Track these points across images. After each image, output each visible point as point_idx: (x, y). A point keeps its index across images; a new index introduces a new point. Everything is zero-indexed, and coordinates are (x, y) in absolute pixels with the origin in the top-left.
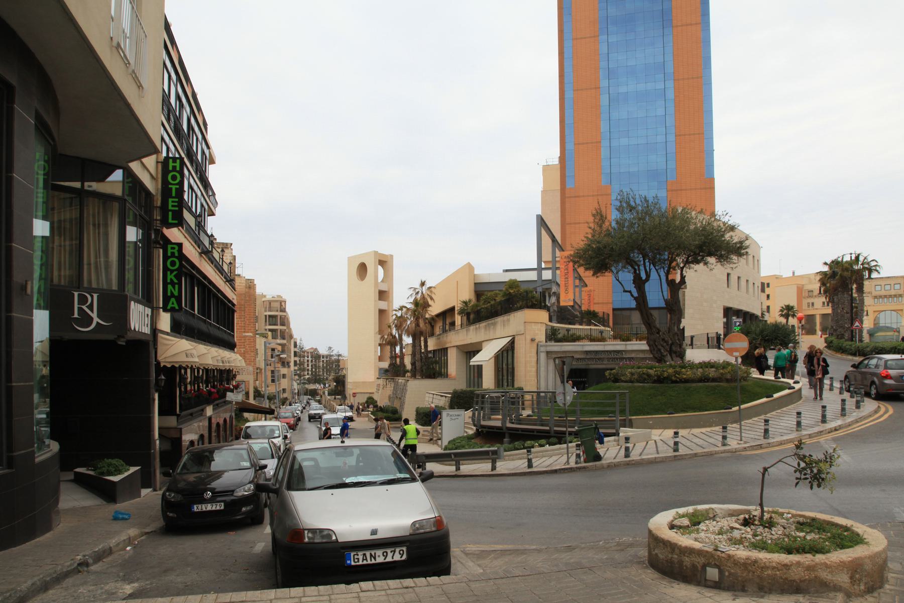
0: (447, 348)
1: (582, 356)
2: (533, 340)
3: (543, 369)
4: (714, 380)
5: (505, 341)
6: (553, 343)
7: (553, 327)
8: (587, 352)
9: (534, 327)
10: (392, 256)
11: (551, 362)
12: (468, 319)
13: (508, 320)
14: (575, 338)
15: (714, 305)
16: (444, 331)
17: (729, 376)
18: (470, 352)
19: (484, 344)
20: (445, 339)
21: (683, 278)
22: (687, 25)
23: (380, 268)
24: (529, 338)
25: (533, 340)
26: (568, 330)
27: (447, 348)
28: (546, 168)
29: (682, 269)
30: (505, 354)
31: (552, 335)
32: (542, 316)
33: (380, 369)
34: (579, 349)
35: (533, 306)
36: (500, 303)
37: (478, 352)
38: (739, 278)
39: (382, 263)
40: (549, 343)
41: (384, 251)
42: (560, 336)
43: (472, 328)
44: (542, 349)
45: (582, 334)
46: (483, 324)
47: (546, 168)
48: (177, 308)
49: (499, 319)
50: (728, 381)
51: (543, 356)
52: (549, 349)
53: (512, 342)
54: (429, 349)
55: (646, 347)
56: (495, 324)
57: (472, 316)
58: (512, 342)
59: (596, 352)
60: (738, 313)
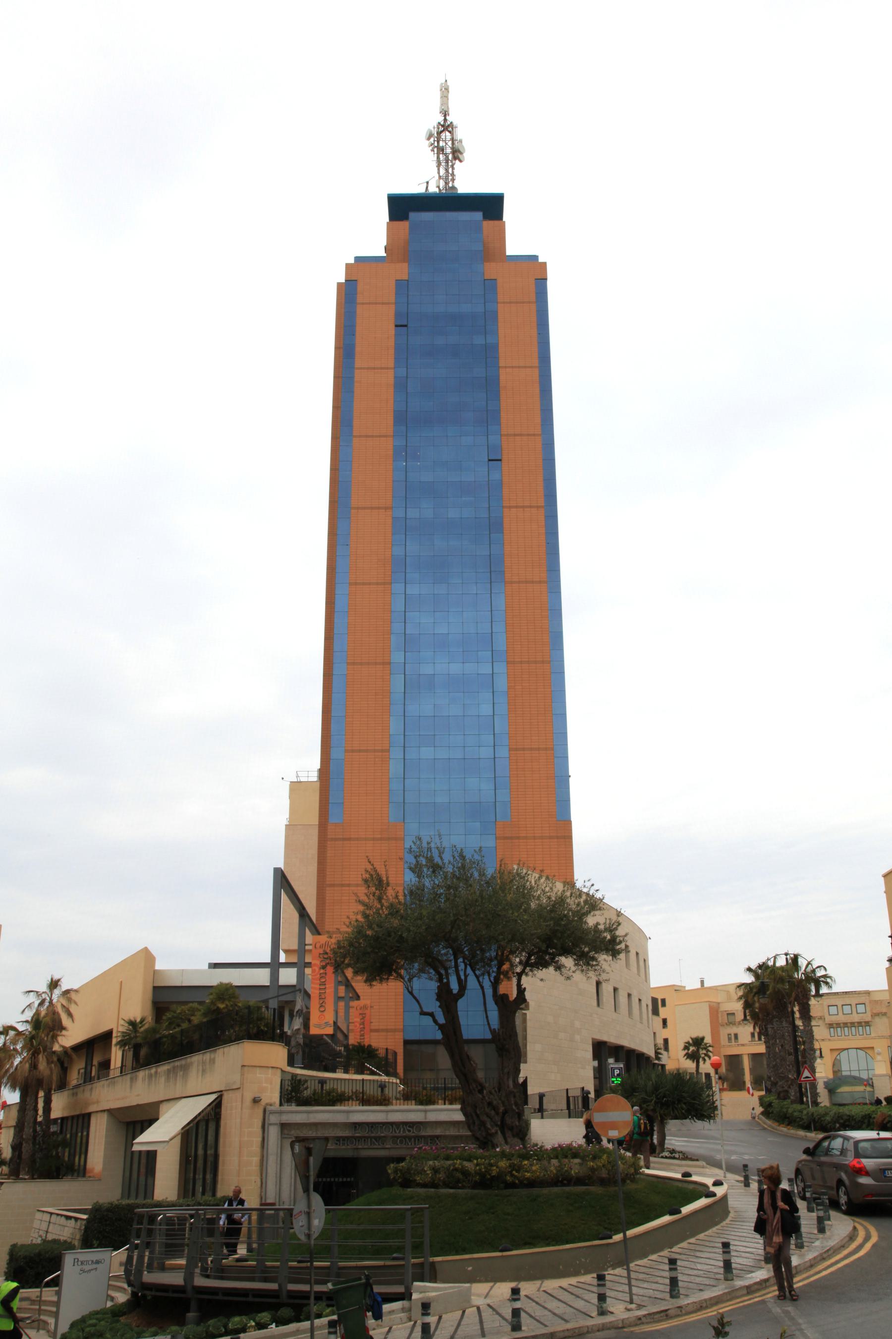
1: (347, 1133)
2: (256, 1101)
4: (580, 1181)
5: (204, 1102)
6: (294, 1108)
7: (294, 1076)
8: (356, 1125)
9: (260, 1075)
12: (136, 1056)
13: (213, 1061)
14: (334, 1098)
16: (88, 1079)
18: (134, 1123)
19: (163, 1107)
20: (87, 1094)
21: (521, 991)
26: (322, 1082)
28: (296, 787)
30: (202, 1128)
31: (293, 1093)
34: (340, 1118)
36: (199, 1027)
37: (157, 1119)
40: (286, 1108)
42: (307, 1093)
43: (142, 1074)
44: (273, 1119)
45: (348, 1090)
46: (164, 1068)
49: (196, 1059)
51: (274, 1133)
54: (54, 1115)
56: (186, 1068)
57: (143, 1052)
58: (216, 1109)
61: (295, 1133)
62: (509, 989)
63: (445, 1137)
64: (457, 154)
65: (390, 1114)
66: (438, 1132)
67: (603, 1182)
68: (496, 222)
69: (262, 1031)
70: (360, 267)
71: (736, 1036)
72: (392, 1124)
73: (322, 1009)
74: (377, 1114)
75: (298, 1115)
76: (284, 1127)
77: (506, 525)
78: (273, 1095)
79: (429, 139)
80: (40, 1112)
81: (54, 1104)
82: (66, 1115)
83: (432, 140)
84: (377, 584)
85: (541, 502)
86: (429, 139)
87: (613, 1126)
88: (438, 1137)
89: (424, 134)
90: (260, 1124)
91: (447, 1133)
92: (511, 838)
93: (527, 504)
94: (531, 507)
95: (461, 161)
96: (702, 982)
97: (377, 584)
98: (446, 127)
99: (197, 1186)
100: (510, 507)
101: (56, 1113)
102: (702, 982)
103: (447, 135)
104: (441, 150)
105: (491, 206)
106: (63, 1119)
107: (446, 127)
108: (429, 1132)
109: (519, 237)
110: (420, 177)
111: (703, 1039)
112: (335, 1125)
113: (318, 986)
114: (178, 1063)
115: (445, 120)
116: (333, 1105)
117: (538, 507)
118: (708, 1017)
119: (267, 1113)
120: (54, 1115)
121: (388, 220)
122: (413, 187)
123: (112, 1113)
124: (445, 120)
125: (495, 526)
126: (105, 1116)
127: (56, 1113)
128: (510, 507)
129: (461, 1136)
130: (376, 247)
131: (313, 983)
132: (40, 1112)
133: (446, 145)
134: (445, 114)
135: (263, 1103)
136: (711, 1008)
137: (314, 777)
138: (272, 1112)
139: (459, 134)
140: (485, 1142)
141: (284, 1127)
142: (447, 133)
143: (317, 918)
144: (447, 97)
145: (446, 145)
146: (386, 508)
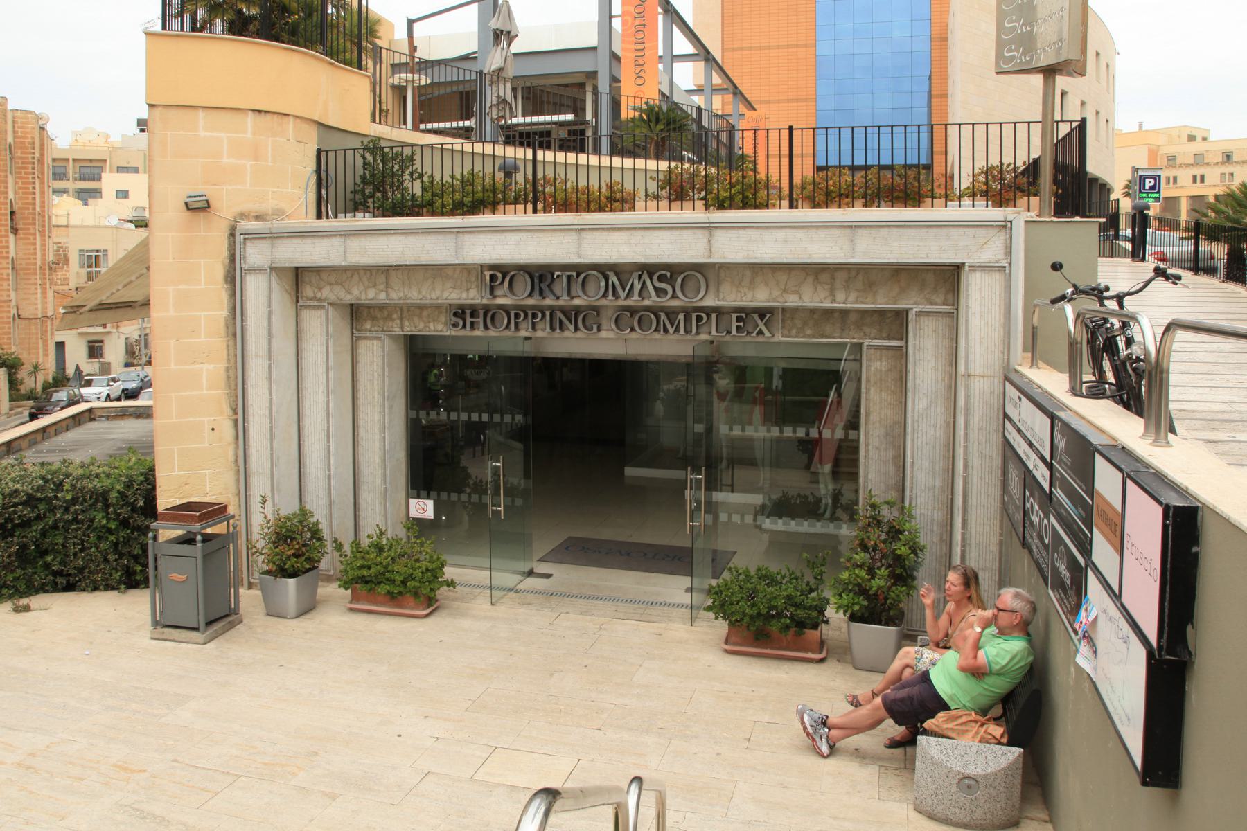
1: (473, 296)
8: (499, 274)
44: (256, 254)
63: (789, 314)
65: (588, 237)
66: (760, 297)
71: (1175, 178)
72: (603, 269)
73: (639, 81)
74: (547, 238)
88: (762, 313)
90: (219, 272)
91: (792, 301)
96: (1141, 126)
102: (1141, 126)
108: (729, 297)
111: (225, 507)
112: (436, 271)
113: (633, 47)
116: (418, 215)
119: (239, 239)
129: (844, 313)
131: (623, 42)
136: (1150, 151)
138: (250, 237)
143: (695, 15)
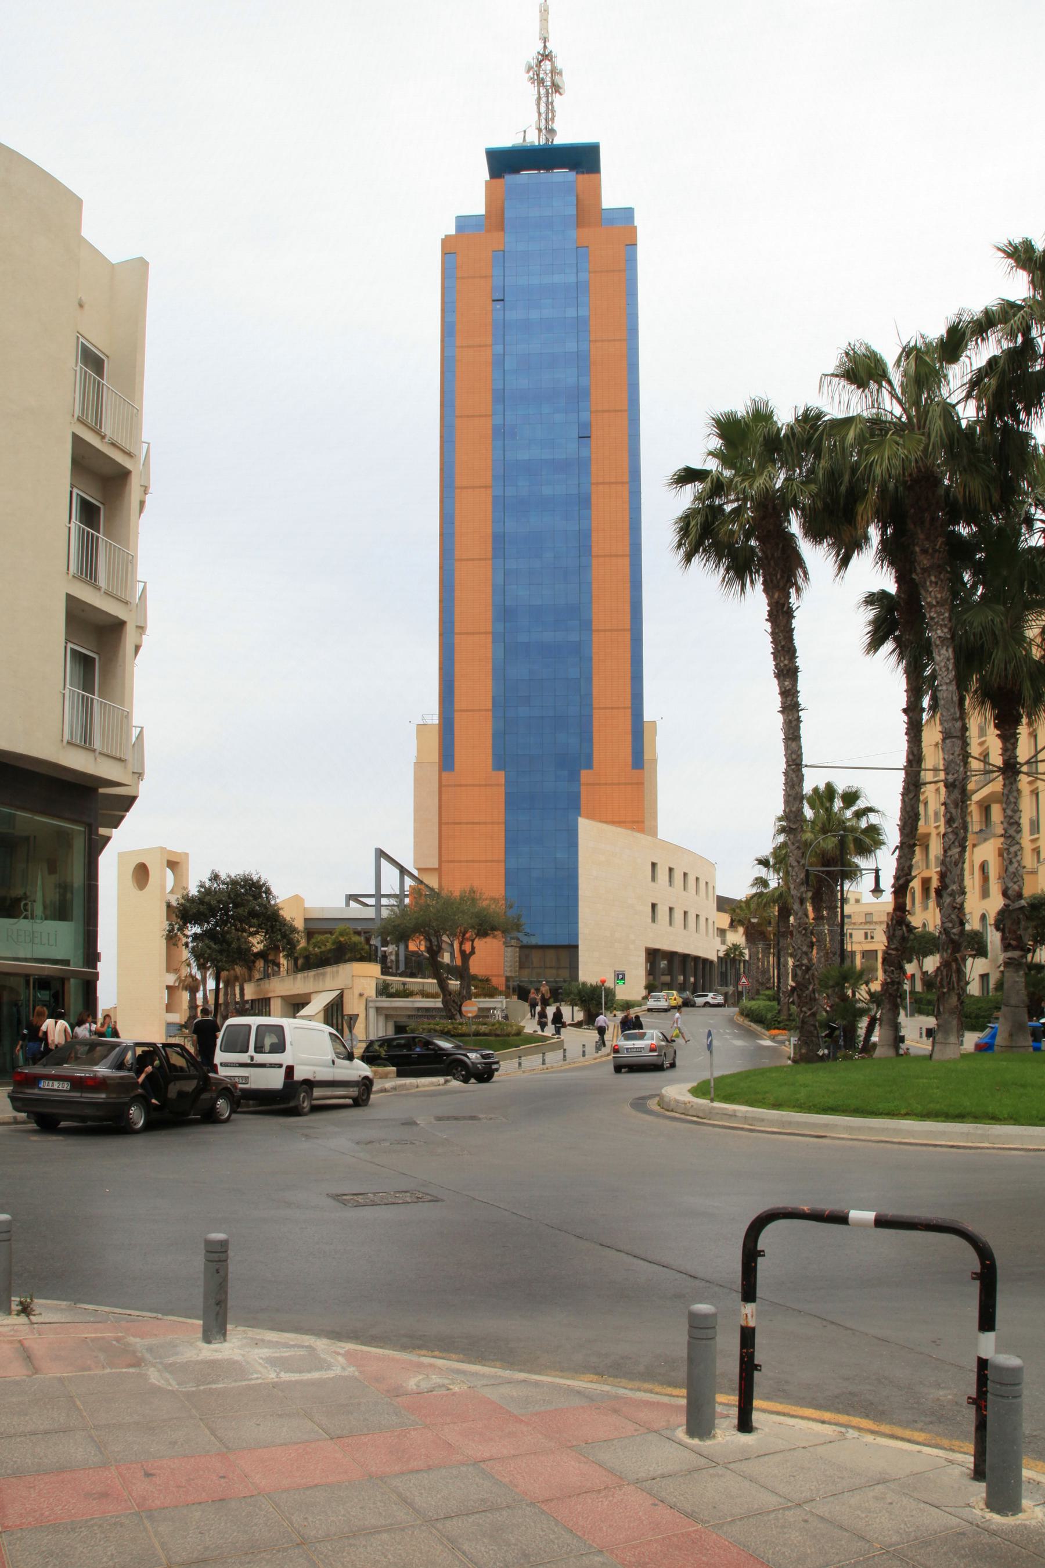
0: (269, 999)
1: (413, 1013)
2: (361, 995)
3: (371, 1026)
4: (485, 1034)
5: (333, 995)
6: (384, 998)
7: (384, 981)
8: (419, 1009)
9: (363, 981)
10: (187, 854)
11: (382, 1019)
12: (296, 964)
13: (338, 972)
14: (406, 994)
15: (632, 947)
16: (267, 976)
17: (498, 1032)
18: (298, 1005)
19: (313, 996)
20: (267, 986)
21: (473, 948)
22: (611, 556)
23: (169, 871)
24: (356, 992)
25: (361, 995)
26: (404, 984)
27: (269, 999)
28: (422, 728)
29: (473, 941)
30: (335, 1008)
31: (384, 990)
32: (374, 969)
33: (169, 1025)
34: (410, 1005)
35: (362, 959)
36: (330, 950)
37: (307, 1004)
38: (671, 909)
39: (172, 865)
40: (380, 999)
41: (176, 846)
42: (393, 990)
43: (300, 976)
44: (371, 1004)
45: (415, 988)
46: (312, 973)
47: (422, 728)
48: (657, 1099)
49: (329, 970)
50: (497, 1035)
51: (372, 1012)
52: (379, 1005)
53: (341, 996)
54: (247, 997)
55: (440, 1005)
56: (324, 974)
57: (300, 962)
58: (341, 996)
59: (427, 1009)
60: (671, 956)
61: (385, 1012)
62: (467, 947)
64: (556, 88)
67: (497, 1035)
68: (592, 176)
69: (173, 1067)
70: (463, 222)
75: (386, 1002)
76: (378, 1010)
77: (594, 500)
78: (371, 991)
79: (528, 72)
80: (238, 996)
81: (246, 992)
82: (254, 997)
83: (531, 73)
84: (480, 559)
85: (626, 478)
86: (528, 72)
87: (470, 1012)
89: (523, 69)
92: (594, 784)
93: (613, 480)
94: (616, 483)
95: (561, 94)
97: (480, 559)
98: (546, 56)
99: (841, 1421)
100: (598, 484)
101: (248, 997)
103: (547, 65)
104: (541, 82)
105: (584, 159)
106: (252, 1000)
107: (546, 56)
109: (614, 189)
110: (518, 130)
114: (321, 970)
115: (545, 47)
117: (623, 483)
118: (580, 959)
120: (247, 997)
121: (487, 176)
122: (508, 140)
123: (284, 998)
124: (545, 47)
125: (584, 501)
126: (279, 1000)
127: (248, 997)
128: (598, 484)
130: (477, 206)
132: (238, 996)
133: (546, 77)
134: (545, 40)
135: (365, 996)
137: (436, 720)
139: (559, 64)
140: (452, 1017)
141: (378, 1010)
142: (548, 63)
144: (546, 20)
145: (546, 77)
146: (486, 487)
